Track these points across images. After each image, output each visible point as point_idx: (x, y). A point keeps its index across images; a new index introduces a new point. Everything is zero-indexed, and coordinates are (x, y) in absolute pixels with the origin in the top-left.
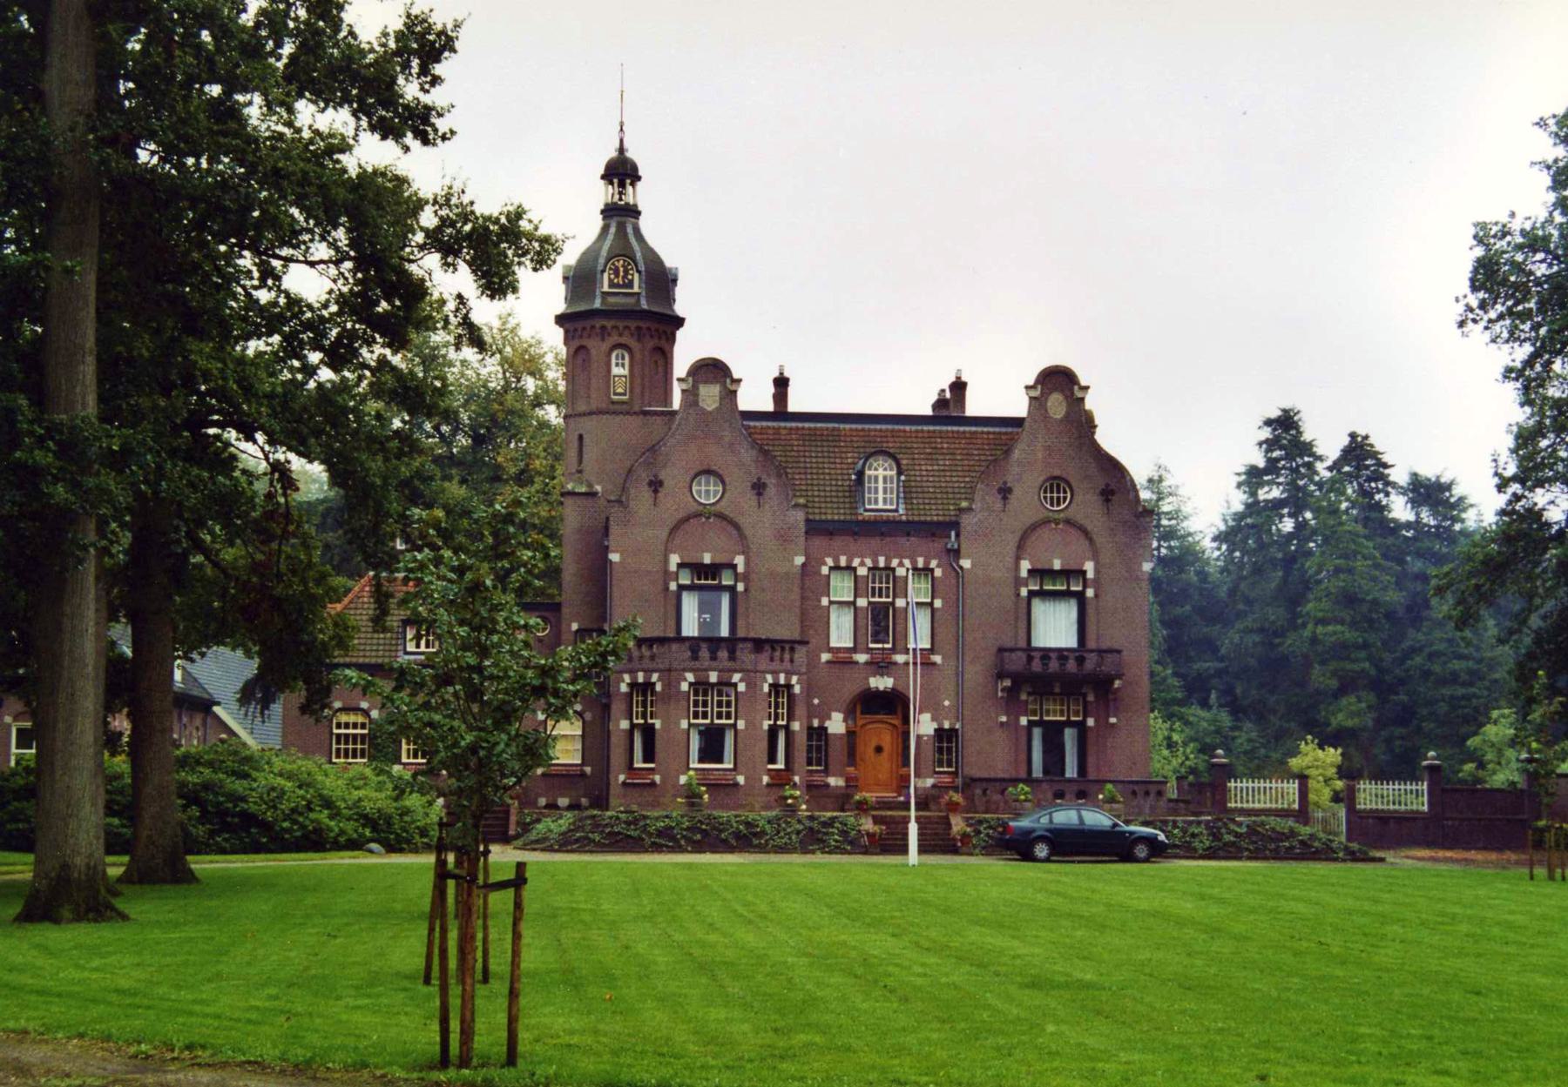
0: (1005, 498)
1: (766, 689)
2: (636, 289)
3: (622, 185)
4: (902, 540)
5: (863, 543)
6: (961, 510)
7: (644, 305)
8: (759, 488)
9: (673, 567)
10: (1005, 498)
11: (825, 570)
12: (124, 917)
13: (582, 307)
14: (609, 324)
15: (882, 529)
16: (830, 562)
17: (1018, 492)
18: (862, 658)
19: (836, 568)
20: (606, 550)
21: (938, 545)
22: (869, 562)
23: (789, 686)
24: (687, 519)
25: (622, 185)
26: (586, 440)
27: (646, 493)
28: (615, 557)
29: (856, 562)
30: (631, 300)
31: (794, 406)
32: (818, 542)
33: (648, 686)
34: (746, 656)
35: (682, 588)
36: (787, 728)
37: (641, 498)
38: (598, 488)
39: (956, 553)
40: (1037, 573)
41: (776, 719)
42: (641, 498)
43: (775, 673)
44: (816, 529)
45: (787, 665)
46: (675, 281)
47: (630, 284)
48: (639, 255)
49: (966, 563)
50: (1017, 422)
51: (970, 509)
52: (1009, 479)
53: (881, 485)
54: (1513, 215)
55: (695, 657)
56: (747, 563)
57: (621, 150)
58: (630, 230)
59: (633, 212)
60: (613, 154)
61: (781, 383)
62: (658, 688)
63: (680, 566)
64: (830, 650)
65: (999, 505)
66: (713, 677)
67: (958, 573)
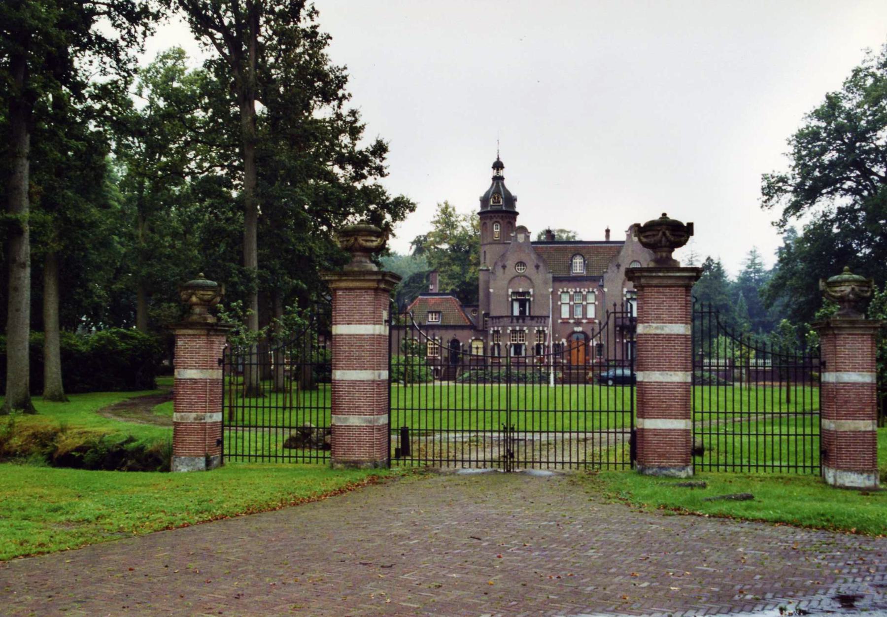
0: (618, 268)
1: (535, 332)
2: (501, 203)
3: (498, 170)
4: (585, 283)
5: (571, 284)
6: (604, 272)
7: (504, 208)
8: (537, 267)
9: (625, 293)
10: (618, 268)
11: (559, 293)
12: (68, 401)
13: (485, 210)
14: (493, 215)
15: (578, 279)
16: (561, 290)
17: (508, 267)
18: (572, 321)
19: (563, 292)
20: (489, 288)
21: (596, 284)
22: (574, 290)
23: (544, 331)
24: (514, 278)
25: (498, 170)
26: (487, 252)
27: (501, 270)
28: (491, 290)
29: (569, 290)
30: (500, 207)
31: (612, 239)
32: (557, 284)
33: (498, 332)
34: (528, 321)
35: (513, 300)
36: (544, 344)
37: (499, 271)
38: (490, 268)
39: (602, 286)
40: (513, 293)
41: (540, 341)
42: (499, 271)
43: (538, 327)
44: (556, 279)
45: (543, 324)
46: (516, 200)
47: (499, 202)
48: (502, 193)
49: (606, 290)
50: (623, 242)
51: (606, 272)
52: (620, 261)
53: (578, 265)
54: (774, 171)
55: (512, 322)
56: (534, 291)
57: (498, 159)
58: (500, 184)
59: (502, 178)
60: (495, 160)
61: (608, 231)
62: (501, 332)
63: (627, 292)
64: (561, 319)
65: (616, 271)
66: (518, 328)
67: (603, 293)
